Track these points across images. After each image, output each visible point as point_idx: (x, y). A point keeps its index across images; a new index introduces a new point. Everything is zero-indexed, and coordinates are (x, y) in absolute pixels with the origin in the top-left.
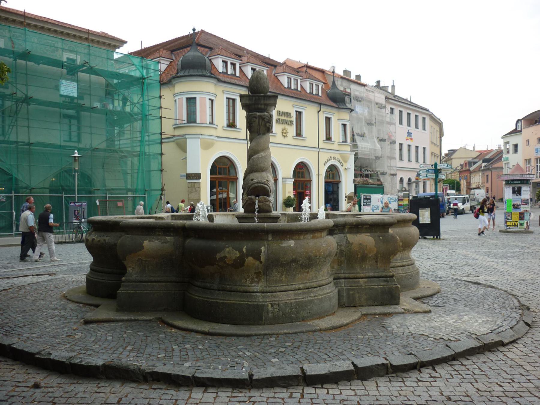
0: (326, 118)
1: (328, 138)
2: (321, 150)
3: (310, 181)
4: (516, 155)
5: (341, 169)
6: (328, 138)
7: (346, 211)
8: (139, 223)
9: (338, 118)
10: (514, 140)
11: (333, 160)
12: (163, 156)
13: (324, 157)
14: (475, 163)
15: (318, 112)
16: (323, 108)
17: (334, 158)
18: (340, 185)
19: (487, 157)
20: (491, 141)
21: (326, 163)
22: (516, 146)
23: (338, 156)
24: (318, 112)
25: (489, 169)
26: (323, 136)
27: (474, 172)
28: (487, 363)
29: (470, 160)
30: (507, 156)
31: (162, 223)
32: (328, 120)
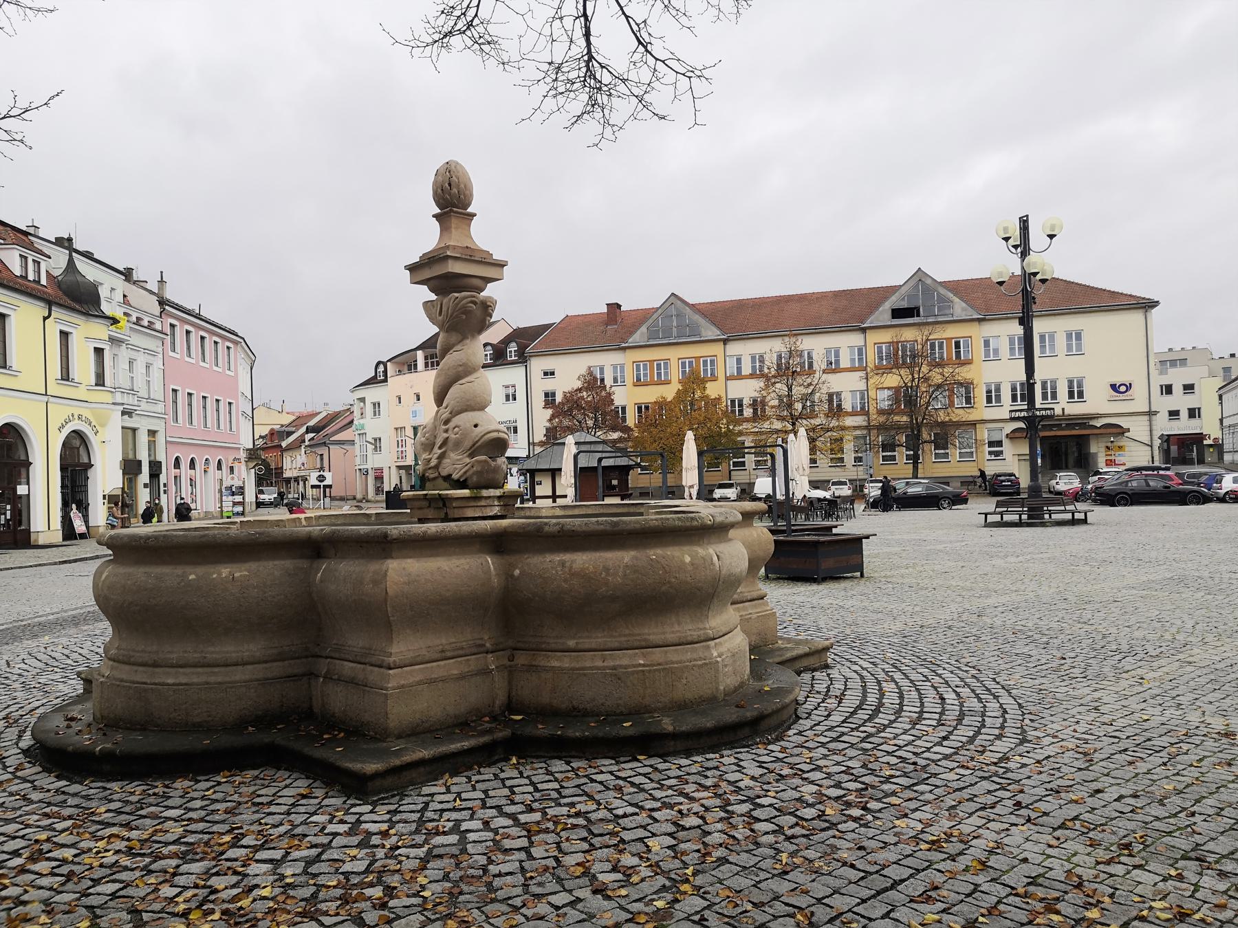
0: (61, 332)
1: (66, 376)
2: (52, 399)
3: (27, 464)
4: (376, 421)
5: (94, 441)
6: (66, 376)
7: (774, 477)
8: (529, 524)
9: (87, 334)
10: (372, 394)
11: (76, 421)
12: (1057, 262)
13: (59, 413)
14: (289, 434)
15: (45, 319)
16: (57, 312)
17: (80, 417)
18: (90, 473)
19: (311, 423)
20: (328, 396)
21: (63, 426)
22: (376, 405)
23: (86, 413)
24: (45, 319)
25: (324, 444)
26: (55, 370)
27: (289, 448)
28: (980, 806)
29: (277, 427)
30: (362, 421)
31: (637, 522)
32: (64, 335)
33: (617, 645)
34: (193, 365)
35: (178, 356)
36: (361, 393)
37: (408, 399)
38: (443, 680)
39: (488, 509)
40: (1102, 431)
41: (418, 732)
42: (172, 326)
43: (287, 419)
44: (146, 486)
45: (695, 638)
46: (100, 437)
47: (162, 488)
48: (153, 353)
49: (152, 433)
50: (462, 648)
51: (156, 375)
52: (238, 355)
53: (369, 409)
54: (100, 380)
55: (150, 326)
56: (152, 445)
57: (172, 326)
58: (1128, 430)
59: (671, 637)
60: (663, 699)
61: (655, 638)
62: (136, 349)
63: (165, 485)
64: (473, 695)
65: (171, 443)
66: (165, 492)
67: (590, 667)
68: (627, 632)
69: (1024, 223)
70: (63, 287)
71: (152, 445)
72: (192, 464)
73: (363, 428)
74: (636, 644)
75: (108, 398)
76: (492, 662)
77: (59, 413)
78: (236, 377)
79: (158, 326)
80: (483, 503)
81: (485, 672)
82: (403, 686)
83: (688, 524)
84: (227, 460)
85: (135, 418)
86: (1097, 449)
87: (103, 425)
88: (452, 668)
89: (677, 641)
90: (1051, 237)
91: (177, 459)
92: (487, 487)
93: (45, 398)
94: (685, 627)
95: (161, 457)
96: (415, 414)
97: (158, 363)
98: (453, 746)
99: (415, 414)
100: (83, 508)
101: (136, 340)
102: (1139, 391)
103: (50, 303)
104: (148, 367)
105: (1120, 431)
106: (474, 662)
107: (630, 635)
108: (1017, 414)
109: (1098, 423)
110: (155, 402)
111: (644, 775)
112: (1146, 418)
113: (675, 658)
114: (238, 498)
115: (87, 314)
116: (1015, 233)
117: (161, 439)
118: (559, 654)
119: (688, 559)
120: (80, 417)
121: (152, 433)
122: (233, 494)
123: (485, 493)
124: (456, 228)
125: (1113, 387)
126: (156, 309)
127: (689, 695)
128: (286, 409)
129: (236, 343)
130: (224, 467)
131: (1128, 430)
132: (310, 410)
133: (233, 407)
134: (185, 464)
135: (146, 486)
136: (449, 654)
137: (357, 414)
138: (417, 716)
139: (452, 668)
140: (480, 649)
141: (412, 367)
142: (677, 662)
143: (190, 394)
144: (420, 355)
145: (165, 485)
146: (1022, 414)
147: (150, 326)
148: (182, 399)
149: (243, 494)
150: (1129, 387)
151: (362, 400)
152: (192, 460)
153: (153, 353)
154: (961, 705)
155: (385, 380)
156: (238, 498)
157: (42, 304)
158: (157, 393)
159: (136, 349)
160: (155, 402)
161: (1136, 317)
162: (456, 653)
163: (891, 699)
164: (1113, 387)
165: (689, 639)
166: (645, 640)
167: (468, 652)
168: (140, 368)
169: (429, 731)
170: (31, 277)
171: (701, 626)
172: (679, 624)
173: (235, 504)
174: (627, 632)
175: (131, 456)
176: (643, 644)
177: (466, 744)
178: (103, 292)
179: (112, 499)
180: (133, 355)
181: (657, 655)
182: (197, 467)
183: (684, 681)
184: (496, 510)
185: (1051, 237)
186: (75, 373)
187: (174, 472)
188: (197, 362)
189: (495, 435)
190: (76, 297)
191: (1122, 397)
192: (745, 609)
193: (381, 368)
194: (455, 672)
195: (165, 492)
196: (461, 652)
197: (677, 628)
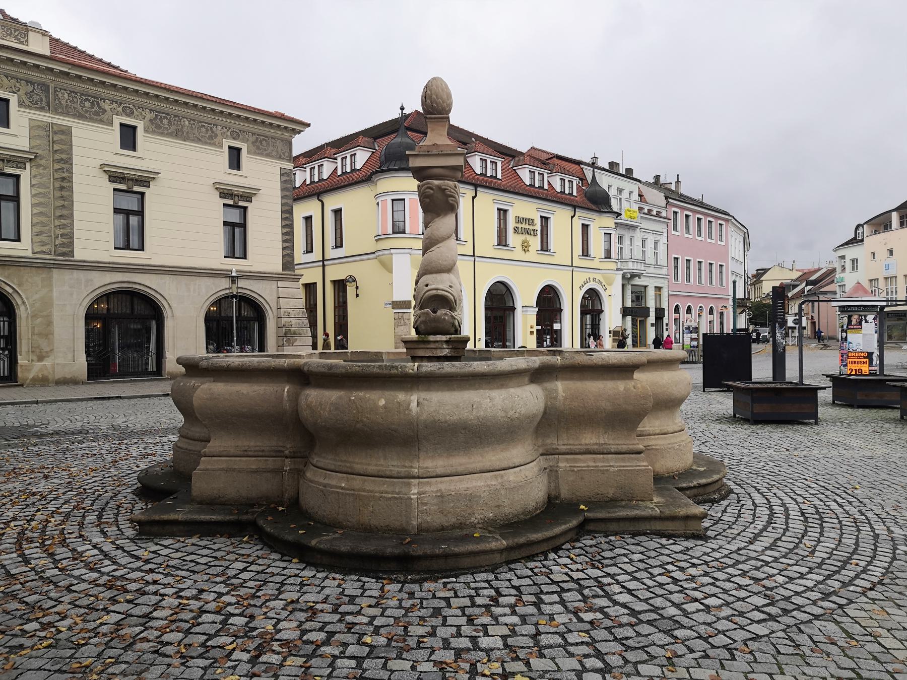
0: (583, 225)
1: (585, 253)
6: (585, 253)
9: (600, 224)
10: (851, 253)
13: (580, 277)
15: (572, 217)
16: (579, 212)
18: (602, 316)
19: (813, 278)
20: (819, 258)
22: (855, 261)
23: (599, 277)
24: (572, 217)
26: (578, 250)
30: (842, 275)
32: (585, 227)
33: (333, 467)
34: (692, 240)
35: (679, 234)
36: (841, 252)
37: (882, 254)
38: (240, 471)
39: (439, 351)
41: (210, 503)
42: (675, 213)
43: (795, 275)
44: (652, 325)
45: (394, 474)
46: (608, 292)
47: (665, 327)
48: (659, 233)
49: (658, 289)
50: (263, 451)
51: (662, 248)
52: (730, 232)
53: (848, 265)
54: (608, 255)
55: (658, 215)
56: (658, 297)
57: (675, 213)
59: (372, 469)
60: (351, 519)
61: (358, 467)
62: (647, 231)
63: (667, 325)
64: (265, 486)
65: (672, 295)
66: (667, 330)
67: (331, 484)
68: (345, 458)
70: (588, 195)
71: (658, 297)
72: (689, 310)
73: (842, 281)
74: (345, 469)
75: (613, 266)
76: (288, 464)
77: (580, 277)
78: (726, 247)
79: (664, 214)
80: (432, 346)
81: (278, 471)
82: (207, 470)
83: (385, 372)
84: (717, 307)
85: (643, 278)
87: (610, 285)
88: (253, 463)
89: (376, 474)
91: (677, 306)
92: (435, 334)
93: (571, 269)
94: (392, 463)
95: (665, 305)
96: (887, 267)
97: (663, 240)
98: (535, 536)
99: (887, 267)
100: (597, 336)
101: (645, 225)
103: (575, 207)
104: (643, 241)
106: (271, 463)
107: (345, 461)
110: (661, 267)
113: (369, 486)
114: (694, 336)
115: (600, 212)
117: (664, 293)
119: (382, 402)
120: (594, 279)
121: (658, 289)
122: (691, 332)
123: (432, 338)
124: (432, 131)
126: (663, 202)
127: (374, 522)
128: (797, 267)
129: (727, 221)
130: (715, 313)
132: (816, 267)
133: (724, 268)
134: (683, 310)
135: (652, 325)
136: (250, 453)
137: (839, 270)
138: (215, 492)
139: (253, 463)
140: (278, 453)
141: (887, 227)
142: (369, 491)
143: (688, 261)
144: (895, 217)
145: (667, 325)
147: (658, 215)
148: (681, 265)
149: (697, 332)
151: (843, 257)
152: (711, 308)
153: (659, 233)
155: (862, 240)
156: (694, 336)
157: (570, 208)
158: (663, 260)
159: (647, 231)
160: (661, 267)
162: (256, 453)
165: (388, 473)
166: (351, 468)
167: (267, 454)
168: (650, 245)
169: (223, 504)
170: (567, 192)
171: (350, 460)
172: (385, 458)
173: (692, 339)
174: (345, 458)
175: (658, 306)
176: (350, 470)
177: (214, 518)
178: (612, 193)
179: (615, 333)
180: (645, 235)
181: (357, 482)
182: (693, 312)
183: (371, 509)
184: (446, 352)
186: (592, 252)
187: (674, 315)
188: (694, 236)
189: (434, 292)
190: (597, 201)
192: (576, 461)
193: (860, 230)
194: (254, 467)
195: (667, 330)
196: (261, 454)
197: (382, 462)
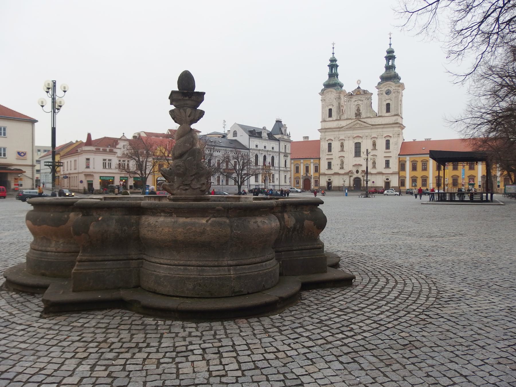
40: (12, 171)
58: (25, 172)
69: (54, 83)
86: (11, 179)
90: (65, 91)
102: (29, 156)
105: (21, 172)
108: (47, 164)
109: (13, 168)
111: (438, 346)
112: (31, 167)
116: (51, 86)
118: (174, 298)
125: (19, 153)
131: (25, 172)
146: (50, 164)
150: (25, 154)
154: (421, 287)
161: (28, 126)
163: (425, 289)
164: (19, 153)
185: (65, 91)
191: (22, 158)
